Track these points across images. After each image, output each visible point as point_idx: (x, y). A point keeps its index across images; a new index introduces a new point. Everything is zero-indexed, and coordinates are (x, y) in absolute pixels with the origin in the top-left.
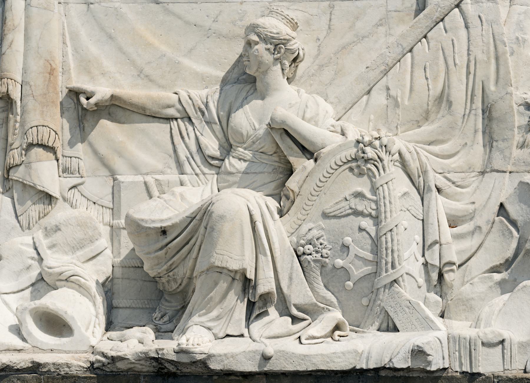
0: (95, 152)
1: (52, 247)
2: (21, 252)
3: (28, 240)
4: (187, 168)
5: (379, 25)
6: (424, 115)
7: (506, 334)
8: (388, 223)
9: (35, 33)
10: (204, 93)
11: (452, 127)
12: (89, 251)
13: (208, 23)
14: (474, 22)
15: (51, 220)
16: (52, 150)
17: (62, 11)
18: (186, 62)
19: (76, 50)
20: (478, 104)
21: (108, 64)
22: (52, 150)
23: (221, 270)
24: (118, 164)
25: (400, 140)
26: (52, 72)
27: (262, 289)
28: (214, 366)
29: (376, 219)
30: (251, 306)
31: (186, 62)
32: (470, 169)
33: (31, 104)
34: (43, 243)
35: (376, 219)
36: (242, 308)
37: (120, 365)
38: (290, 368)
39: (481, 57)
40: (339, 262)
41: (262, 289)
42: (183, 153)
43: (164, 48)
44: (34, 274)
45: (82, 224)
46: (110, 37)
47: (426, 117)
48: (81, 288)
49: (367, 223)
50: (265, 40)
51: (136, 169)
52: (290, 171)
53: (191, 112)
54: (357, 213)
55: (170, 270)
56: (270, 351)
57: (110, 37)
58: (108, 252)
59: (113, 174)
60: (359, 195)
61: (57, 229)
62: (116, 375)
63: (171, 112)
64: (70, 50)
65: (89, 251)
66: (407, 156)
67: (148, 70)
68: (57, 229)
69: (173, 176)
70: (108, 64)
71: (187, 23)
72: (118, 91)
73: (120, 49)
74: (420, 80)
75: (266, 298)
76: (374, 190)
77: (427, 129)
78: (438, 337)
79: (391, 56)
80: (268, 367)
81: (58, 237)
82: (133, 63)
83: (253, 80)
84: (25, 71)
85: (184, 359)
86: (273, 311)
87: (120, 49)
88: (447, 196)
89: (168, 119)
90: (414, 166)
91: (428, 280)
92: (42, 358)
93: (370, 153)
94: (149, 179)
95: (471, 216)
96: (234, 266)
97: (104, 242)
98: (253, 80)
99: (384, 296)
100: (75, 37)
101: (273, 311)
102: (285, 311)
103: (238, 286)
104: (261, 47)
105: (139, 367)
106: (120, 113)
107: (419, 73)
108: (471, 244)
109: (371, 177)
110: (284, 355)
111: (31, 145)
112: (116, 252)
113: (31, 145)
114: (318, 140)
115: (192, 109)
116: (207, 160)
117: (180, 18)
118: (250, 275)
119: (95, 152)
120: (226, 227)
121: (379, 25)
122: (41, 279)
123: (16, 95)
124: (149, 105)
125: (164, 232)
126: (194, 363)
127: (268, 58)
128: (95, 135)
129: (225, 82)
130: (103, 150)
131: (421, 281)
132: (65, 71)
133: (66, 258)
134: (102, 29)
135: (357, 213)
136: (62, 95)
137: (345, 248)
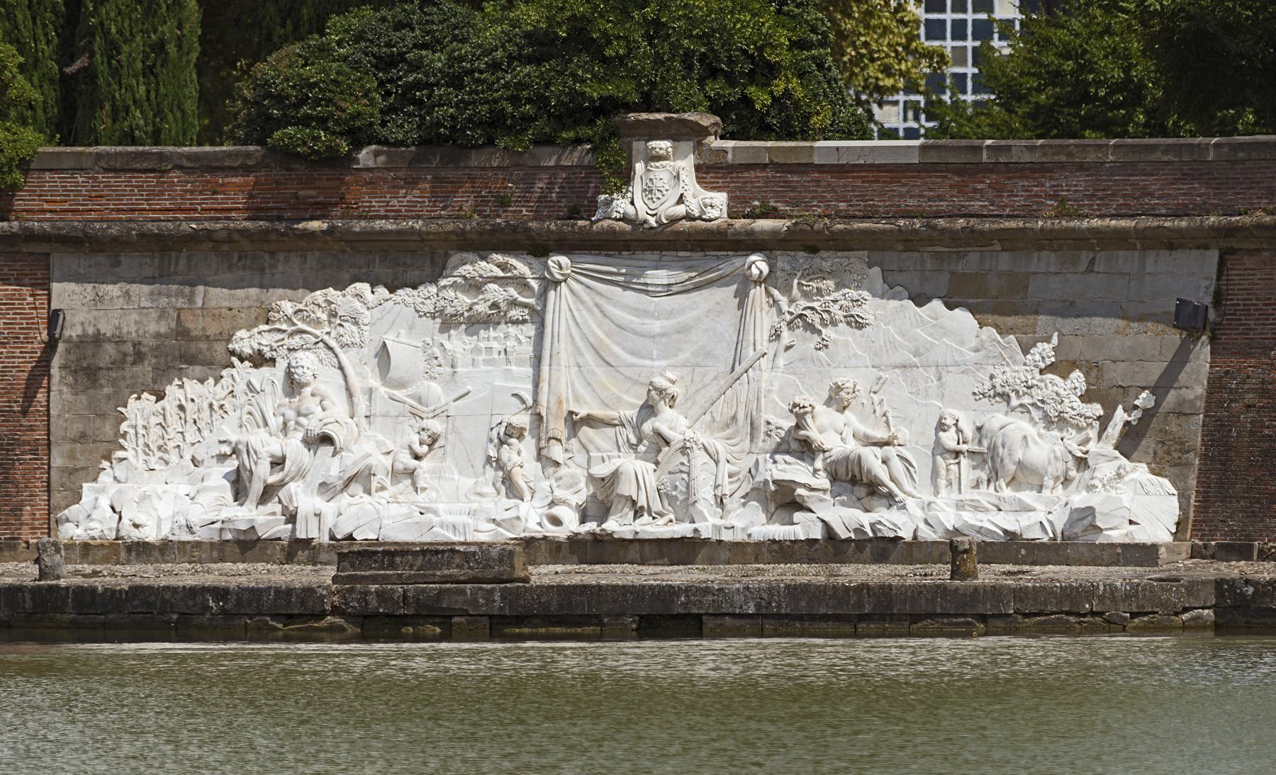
0: (580, 442)
1: (558, 486)
2: (544, 489)
3: (548, 483)
4: (622, 449)
5: (714, 379)
6: (1085, 257)
7: (735, 524)
8: (693, 475)
9: (553, 383)
10: (631, 412)
11: (737, 431)
12: (575, 489)
13: (636, 377)
14: (751, 381)
15: (558, 475)
16: (559, 440)
17: (563, 354)
18: (625, 397)
19: (573, 391)
20: (749, 421)
21: (588, 398)
22: (559, 440)
23: (621, 496)
24: (590, 447)
25: (472, 549)
26: (560, 402)
27: (639, 505)
28: (615, 536)
29: (689, 474)
30: (636, 512)
31: (625, 397)
32: (743, 451)
33: (550, 418)
34: (554, 485)
35: (689, 474)
36: (631, 514)
37: (580, 537)
38: (647, 537)
39: (752, 398)
40: (674, 493)
41: (639, 505)
42: (621, 442)
43: (614, 390)
44: (550, 499)
45: (572, 476)
46: (589, 384)
47: (728, 426)
48: (569, 505)
49: (685, 476)
50: (655, 389)
51: (599, 450)
52: (659, 451)
53: (625, 422)
54: (681, 472)
55: (607, 497)
56: (638, 530)
57: (589, 384)
58: (585, 489)
59: (588, 452)
60: (682, 464)
61: (561, 478)
62: (578, 541)
63: (616, 422)
64: (570, 391)
65: (575, 489)
66: (707, 446)
67: (606, 401)
68: (561, 478)
69: (616, 453)
70: (588, 398)
71: (626, 377)
72: (591, 412)
73: (594, 390)
74: (725, 409)
75: (642, 508)
76: (689, 461)
77: (728, 431)
78: (826, 519)
79: (715, 396)
80: (638, 537)
81: (560, 482)
82: (599, 397)
83: (652, 407)
84: (548, 401)
85: (603, 533)
86: (646, 514)
87: (594, 390)
88: (732, 464)
89: (615, 425)
90: (711, 450)
91: (716, 502)
92: (547, 534)
93: (688, 445)
94: (605, 455)
95: (738, 473)
96: (627, 494)
97: (582, 485)
98: (652, 407)
99: (691, 508)
100: (573, 384)
101: (646, 514)
102: (650, 514)
103: (629, 504)
104: (653, 393)
105: (587, 537)
106: (592, 422)
107: (725, 405)
108: (735, 486)
109: (688, 455)
110: (645, 532)
111: (550, 438)
112: (589, 491)
113: (550, 438)
114: (672, 438)
115: (367, 687)
116: (632, 446)
117: (622, 374)
118: (635, 498)
119: (580, 442)
120: (623, 477)
121: (714, 379)
122: (552, 502)
123: (544, 414)
124: (605, 419)
125: (603, 479)
126: (608, 534)
127: (657, 398)
128: (580, 434)
129: (642, 407)
130: (584, 441)
131: (713, 502)
132: (568, 401)
133: (565, 492)
134: (586, 380)
135: (681, 472)
136: (565, 414)
137: (676, 487)
